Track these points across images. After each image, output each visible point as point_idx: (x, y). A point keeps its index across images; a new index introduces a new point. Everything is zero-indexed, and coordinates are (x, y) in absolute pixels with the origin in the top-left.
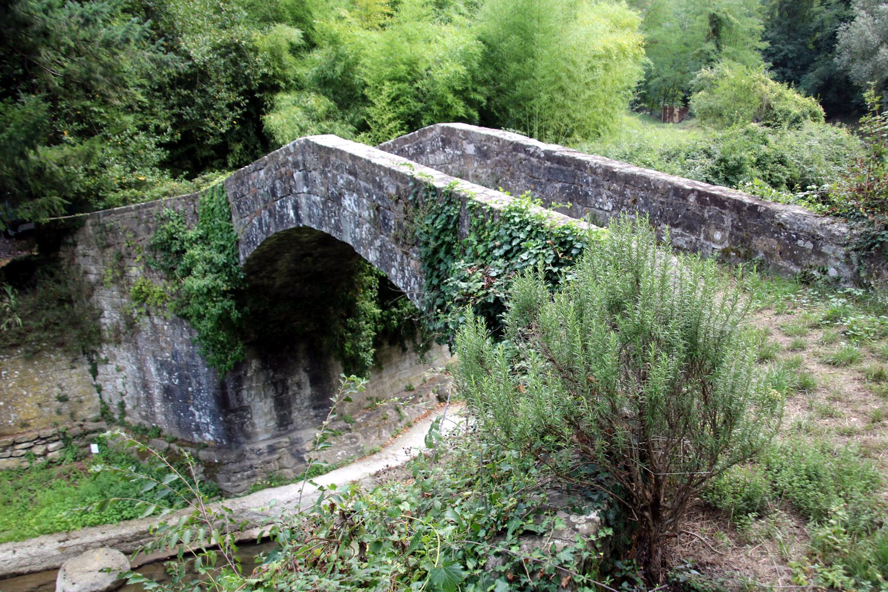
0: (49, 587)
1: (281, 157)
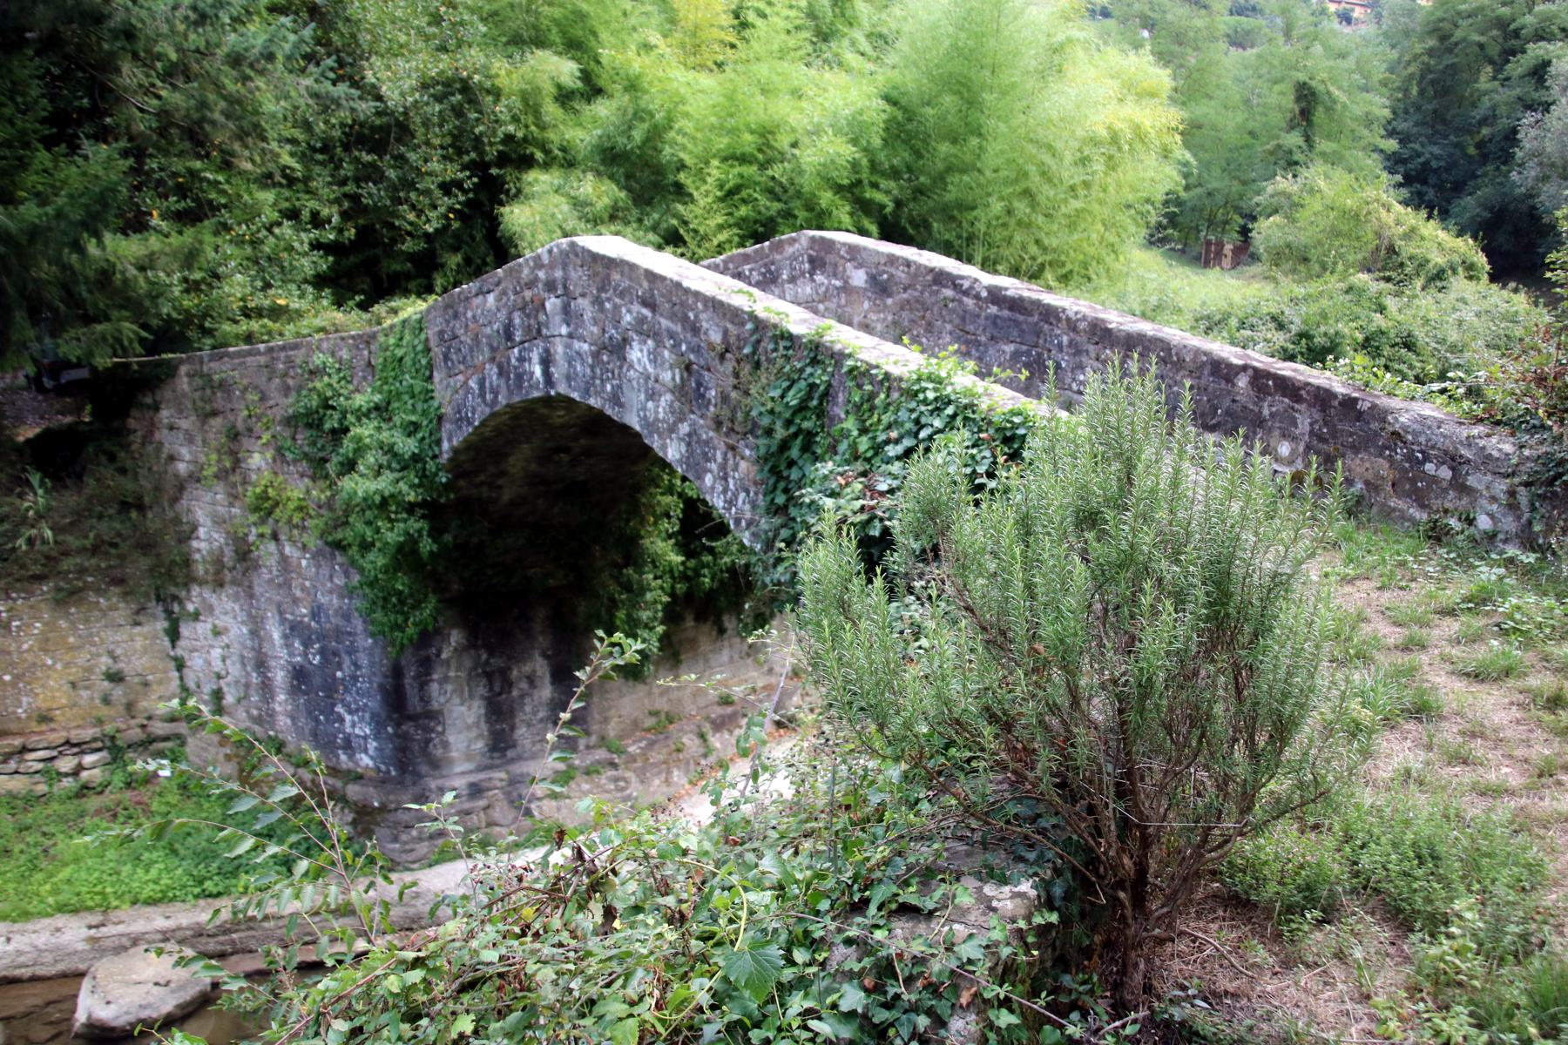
0: (64, 1006)
1: (526, 271)
